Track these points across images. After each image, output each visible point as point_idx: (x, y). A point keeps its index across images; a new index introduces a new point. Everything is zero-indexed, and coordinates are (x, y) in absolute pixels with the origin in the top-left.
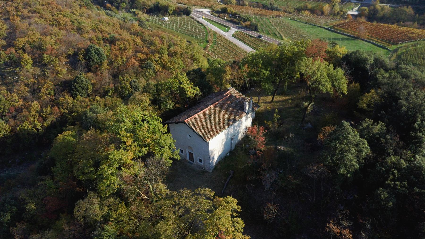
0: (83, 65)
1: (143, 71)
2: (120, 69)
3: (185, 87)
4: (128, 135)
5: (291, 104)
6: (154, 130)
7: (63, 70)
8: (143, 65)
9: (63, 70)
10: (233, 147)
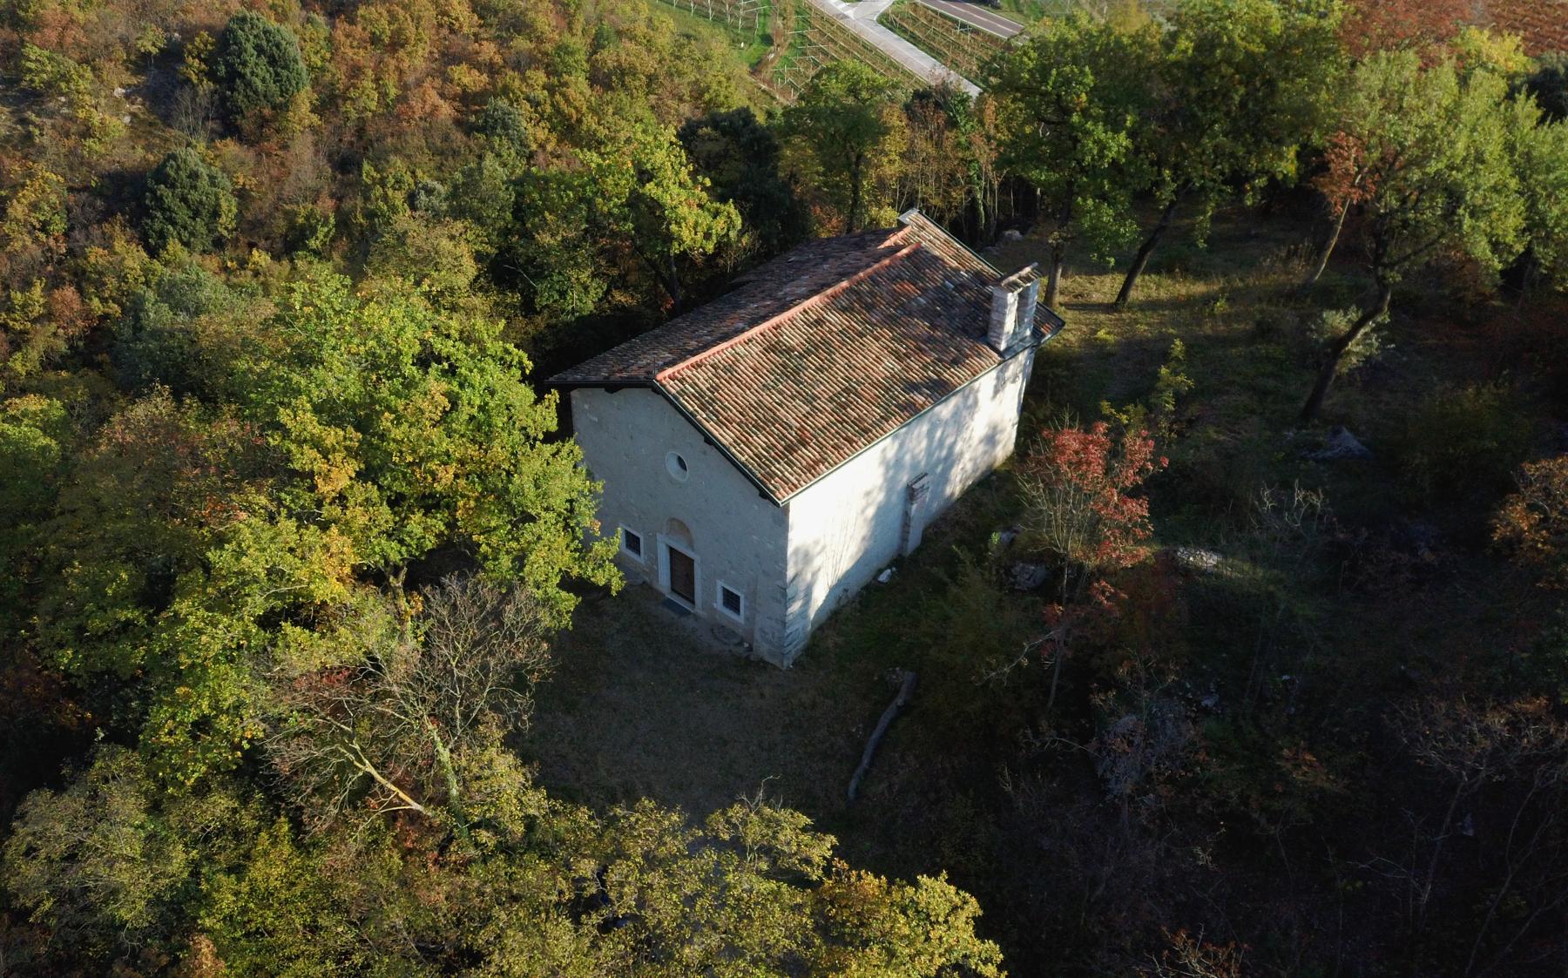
0: (205, 102)
1: (471, 143)
2: (371, 132)
3: (666, 200)
4: (332, 436)
5: (1227, 319)
6: (481, 416)
7: (112, 123)
8: (473, 119)
9: (112, 123)
10: (915, 539)
